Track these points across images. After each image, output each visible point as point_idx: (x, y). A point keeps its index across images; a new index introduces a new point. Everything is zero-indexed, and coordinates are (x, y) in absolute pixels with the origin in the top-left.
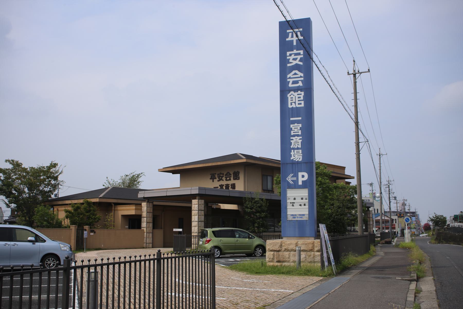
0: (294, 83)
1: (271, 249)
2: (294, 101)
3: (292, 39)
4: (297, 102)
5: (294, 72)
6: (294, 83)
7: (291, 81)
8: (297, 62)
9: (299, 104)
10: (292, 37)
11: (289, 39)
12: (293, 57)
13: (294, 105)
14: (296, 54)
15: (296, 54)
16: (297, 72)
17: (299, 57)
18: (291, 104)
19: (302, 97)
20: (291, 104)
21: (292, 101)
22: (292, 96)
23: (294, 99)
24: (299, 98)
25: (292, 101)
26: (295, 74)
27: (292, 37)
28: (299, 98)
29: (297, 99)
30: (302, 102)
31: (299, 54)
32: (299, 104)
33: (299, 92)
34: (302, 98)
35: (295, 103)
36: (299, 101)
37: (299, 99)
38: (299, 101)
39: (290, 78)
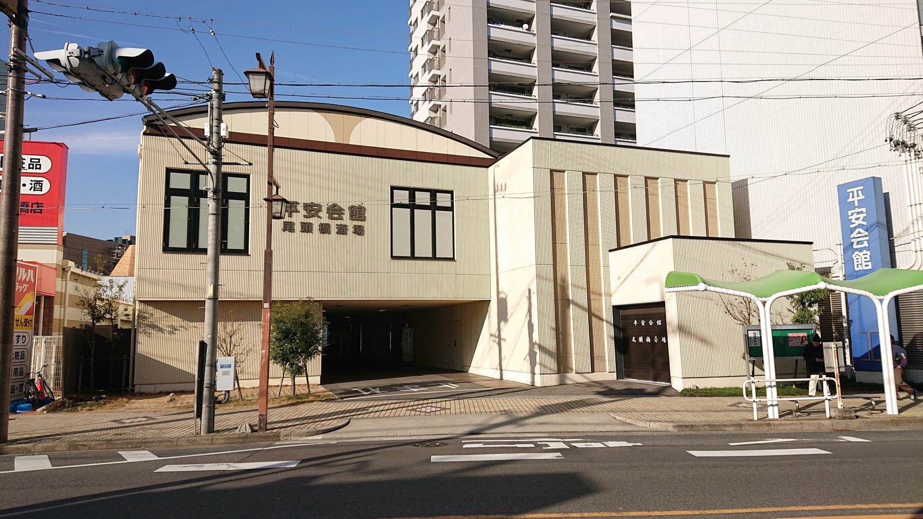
4: (864, 264)
5: (857, 230)
6: (858, 243)
8: (860, 222)
11: (850, 200)
12: (855, 216)
13: (860, 268)
14: (858, 213)
15: (858, 213)
19: (868, 256)
26: (859, 233)
30: (870, 264)
31: (862, 212)
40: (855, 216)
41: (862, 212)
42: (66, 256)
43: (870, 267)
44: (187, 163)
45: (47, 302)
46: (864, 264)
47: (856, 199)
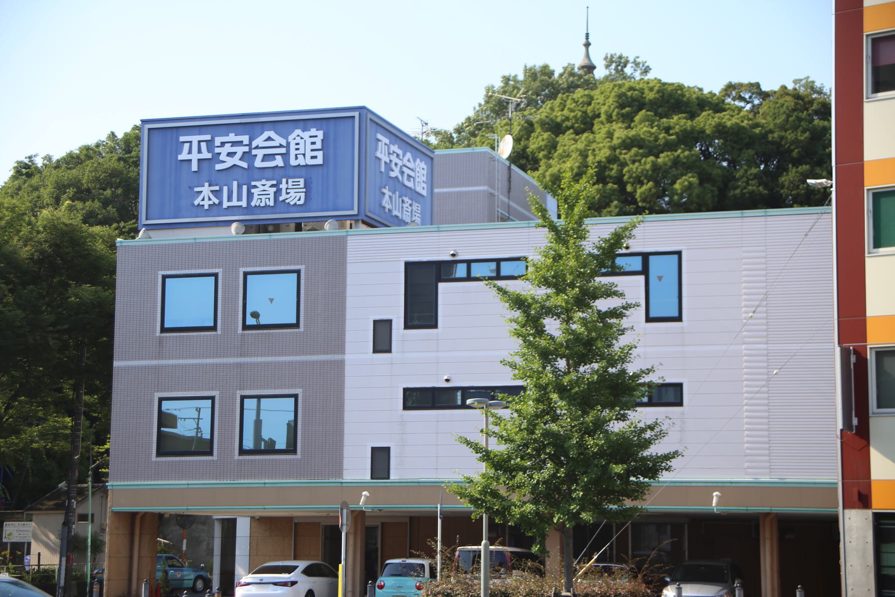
0: (266, 158)
1: (471, 439)
2: (302, 151)
3: (188, 157)
4: (309, 154)
5: (266, 134)
6: (266, 158)
7: (260, 153)
8: (236, 160)
9: (313, 157)
10: (190, 152)
11: (183, 156)
12: (228, 148)
13: (301, 161)
14: (234, 144)
15: (234, 144)
16: (272, 134)
17: (240, 150)
18: (296, 158)
19: (318, 141)
20: (296, 158)
21: (297, 152)
22: (298, 140)
23: (301, 146)
24: (313, 143)
25: (297, 152)
26: (269, 139)
27: (190, 152)
28: (313, 143)
29: (309, 147)
30: (320, 154)
31: (240, 143)
32: (313, 157)
33: (313, 132)
34: (318, 145)
35: (304, 155)
36: (312, 150)
37: (314, 147)
38: (312, 150)
39: (257, 147)
40: (228, 148)
41: (240, 143)
42: (496, 470)
43: (319, 161)
44: (660, 278)
45: (566, 231)
46: (309, 154)
47: (195, 157)
